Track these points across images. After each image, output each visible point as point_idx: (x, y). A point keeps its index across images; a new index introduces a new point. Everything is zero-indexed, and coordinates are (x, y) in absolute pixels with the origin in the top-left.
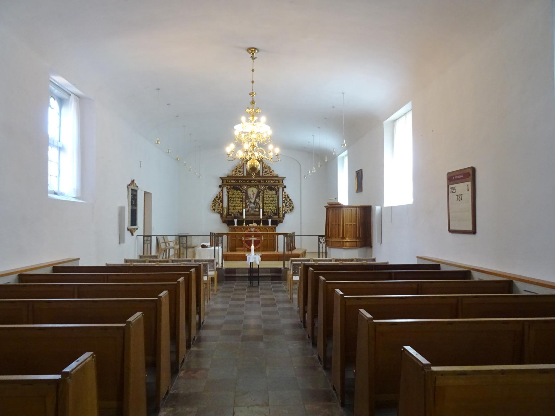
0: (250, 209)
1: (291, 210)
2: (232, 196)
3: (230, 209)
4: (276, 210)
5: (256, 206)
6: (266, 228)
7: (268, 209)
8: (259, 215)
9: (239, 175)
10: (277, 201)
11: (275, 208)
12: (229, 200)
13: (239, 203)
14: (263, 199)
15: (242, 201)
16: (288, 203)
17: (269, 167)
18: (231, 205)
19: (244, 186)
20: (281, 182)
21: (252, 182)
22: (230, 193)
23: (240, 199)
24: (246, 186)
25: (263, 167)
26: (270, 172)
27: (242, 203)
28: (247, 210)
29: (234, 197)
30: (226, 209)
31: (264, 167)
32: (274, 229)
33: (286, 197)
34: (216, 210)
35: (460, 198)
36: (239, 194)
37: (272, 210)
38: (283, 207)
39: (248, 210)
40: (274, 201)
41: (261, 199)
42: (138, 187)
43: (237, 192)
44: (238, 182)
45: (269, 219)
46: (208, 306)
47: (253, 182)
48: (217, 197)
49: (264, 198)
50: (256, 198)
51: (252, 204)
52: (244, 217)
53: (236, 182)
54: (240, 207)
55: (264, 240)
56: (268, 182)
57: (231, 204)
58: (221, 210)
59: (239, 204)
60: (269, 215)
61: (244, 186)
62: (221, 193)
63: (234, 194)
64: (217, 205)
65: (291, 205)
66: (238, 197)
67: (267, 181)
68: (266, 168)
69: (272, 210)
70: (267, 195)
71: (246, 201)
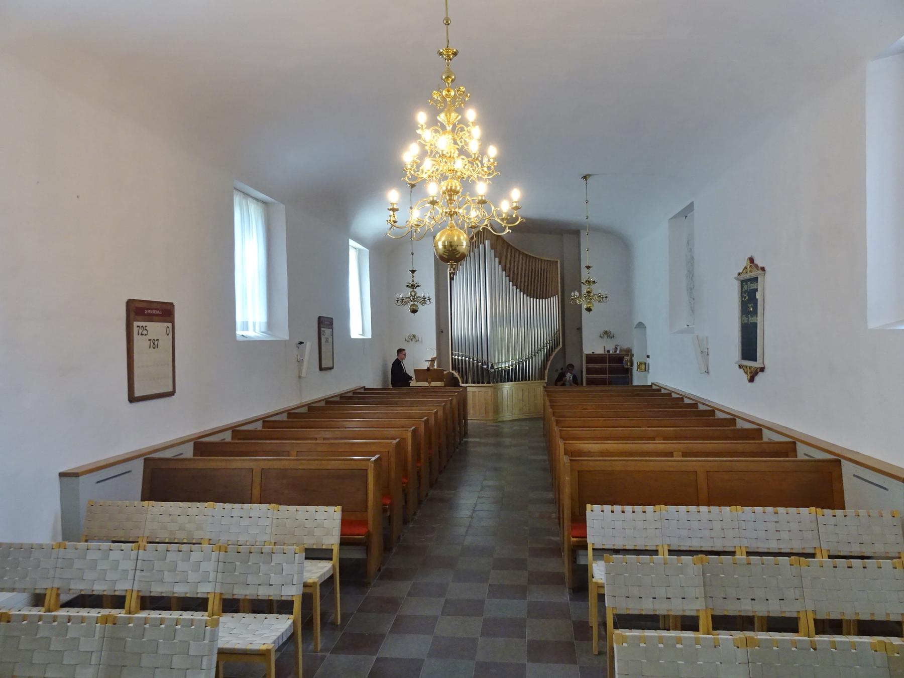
35: (154, 344)
42: (740, 367)
46: (459, 127)
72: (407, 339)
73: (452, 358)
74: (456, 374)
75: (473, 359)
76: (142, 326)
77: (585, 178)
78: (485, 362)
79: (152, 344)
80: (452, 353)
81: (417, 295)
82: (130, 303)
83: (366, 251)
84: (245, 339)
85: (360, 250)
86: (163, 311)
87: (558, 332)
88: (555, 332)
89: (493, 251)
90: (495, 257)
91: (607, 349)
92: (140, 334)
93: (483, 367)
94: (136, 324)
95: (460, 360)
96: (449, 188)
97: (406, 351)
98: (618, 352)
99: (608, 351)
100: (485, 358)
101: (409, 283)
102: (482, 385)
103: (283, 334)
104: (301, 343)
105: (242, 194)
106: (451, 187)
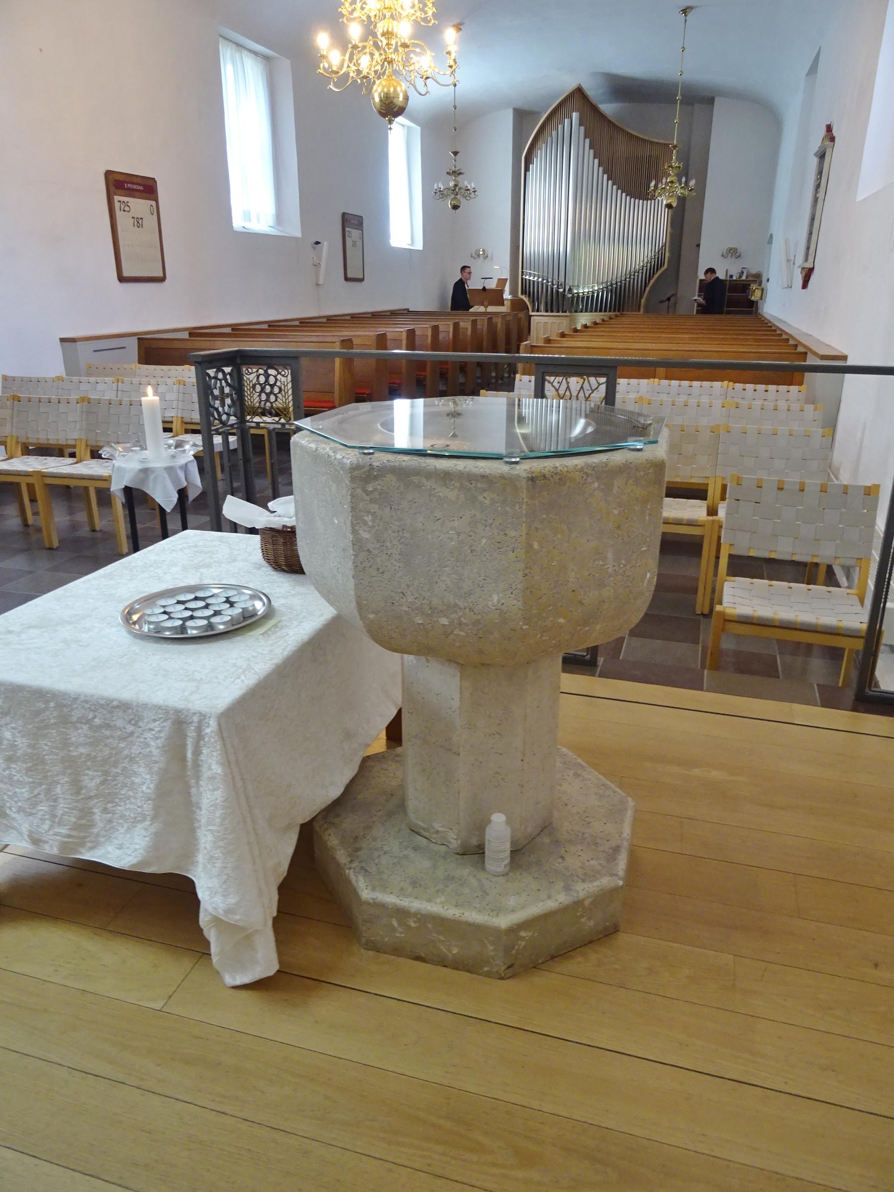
35: (138, 222)
72: (473, 255)
73: (522, 279)
74: (526, 300)
75: (553, 284)
76: (124, 202)
77: (685, 11)
78: (561, 285)
79: (136, 222)
80: (522, 272)
81: (460, 185)
82: (109, 175)
83: (417, 129)
84: (246, 231)
85: (409, 128)
86: (144, 186)
87: (664, 248)
88: (660, 246)
89: (582, 128)
90: (585, 137)
91: (729, 273)
92: (122, 209)
93: (558, 291)
94: (117, 198)
95: (531, 282)
96: (385, 30)
97: (471, 269)
98: (744, 278)
99: (731, 276)
100: (562, 279)
101: (450, 170)
102: (552, 314)
103: (295, 230)
104: (317, 243)
105: (234, 45)
106: (388, 30)
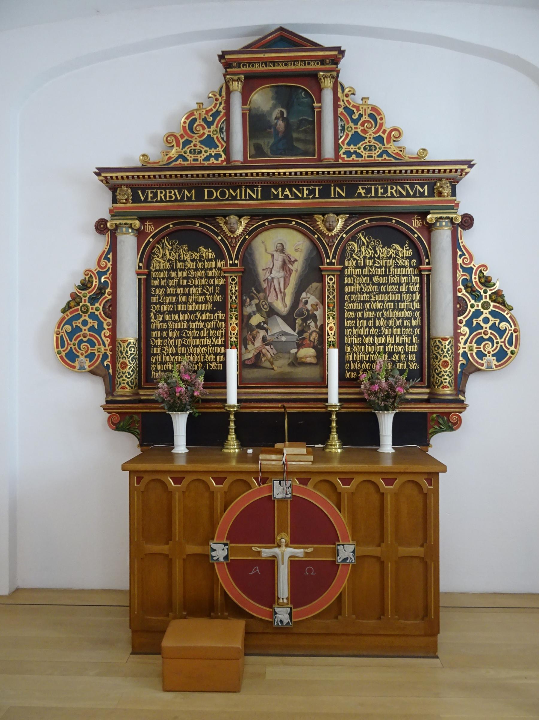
0: (269, 351)
1: (501, 355)
2: (170, 278)
3: (157, 350)
4: (412, 357)
5: (301, 333)
6: (373, 478)
7: (371, 349)
8: (323, 383)
9: (207, 158)
10: (421, 301)
11: (411, 344)
12: (153, 299)
13: (205, 316)
14: (341, 293)
15: (221, 306)
16: (486, 313)
17: (374, 109)
18: (162, 330)
19: (233, 219)
20: (447, 191)
21: (276, 197)
22: (157, 262)
23: (213, 294)
24: (244, 221)
25: (341, 110)
26: (380, 139)
27: (221, 315)
28: (249, 355)
29: (178, 285)
30: (132, 352)
31: (346, 108)
32: (424, 483)
33: (475, 279)
34: (82, 358)
36: (208, 265)
37: (391, 355)
38: (457, 335)
39: (258, 356)
40: (402, 305)
41: (331, 297)
43: (196, 255)
44: (200, 197)
45: (386, 409)
47: (286, 197)
48: (84, 286)
49: (347, 289)
50: (301, 288)
51: (280, 320)
52: (232, 398)
53: (189, 199)
54: (210, 337)
55: (360, 558)
56: (368, 191)
57: (163, 321)
58: (105, 356)
59: (209, 325)
60: (381, 390)
61: (233, 219)
62: (109, 265)
63: (176, 270)
64: (85, 329)
65: (503, 325)
66: (204, 281)
67: (361, 191)
68: (355, 117)
69: (391, 355)
70: (366, 271)
71: (243, 304)
